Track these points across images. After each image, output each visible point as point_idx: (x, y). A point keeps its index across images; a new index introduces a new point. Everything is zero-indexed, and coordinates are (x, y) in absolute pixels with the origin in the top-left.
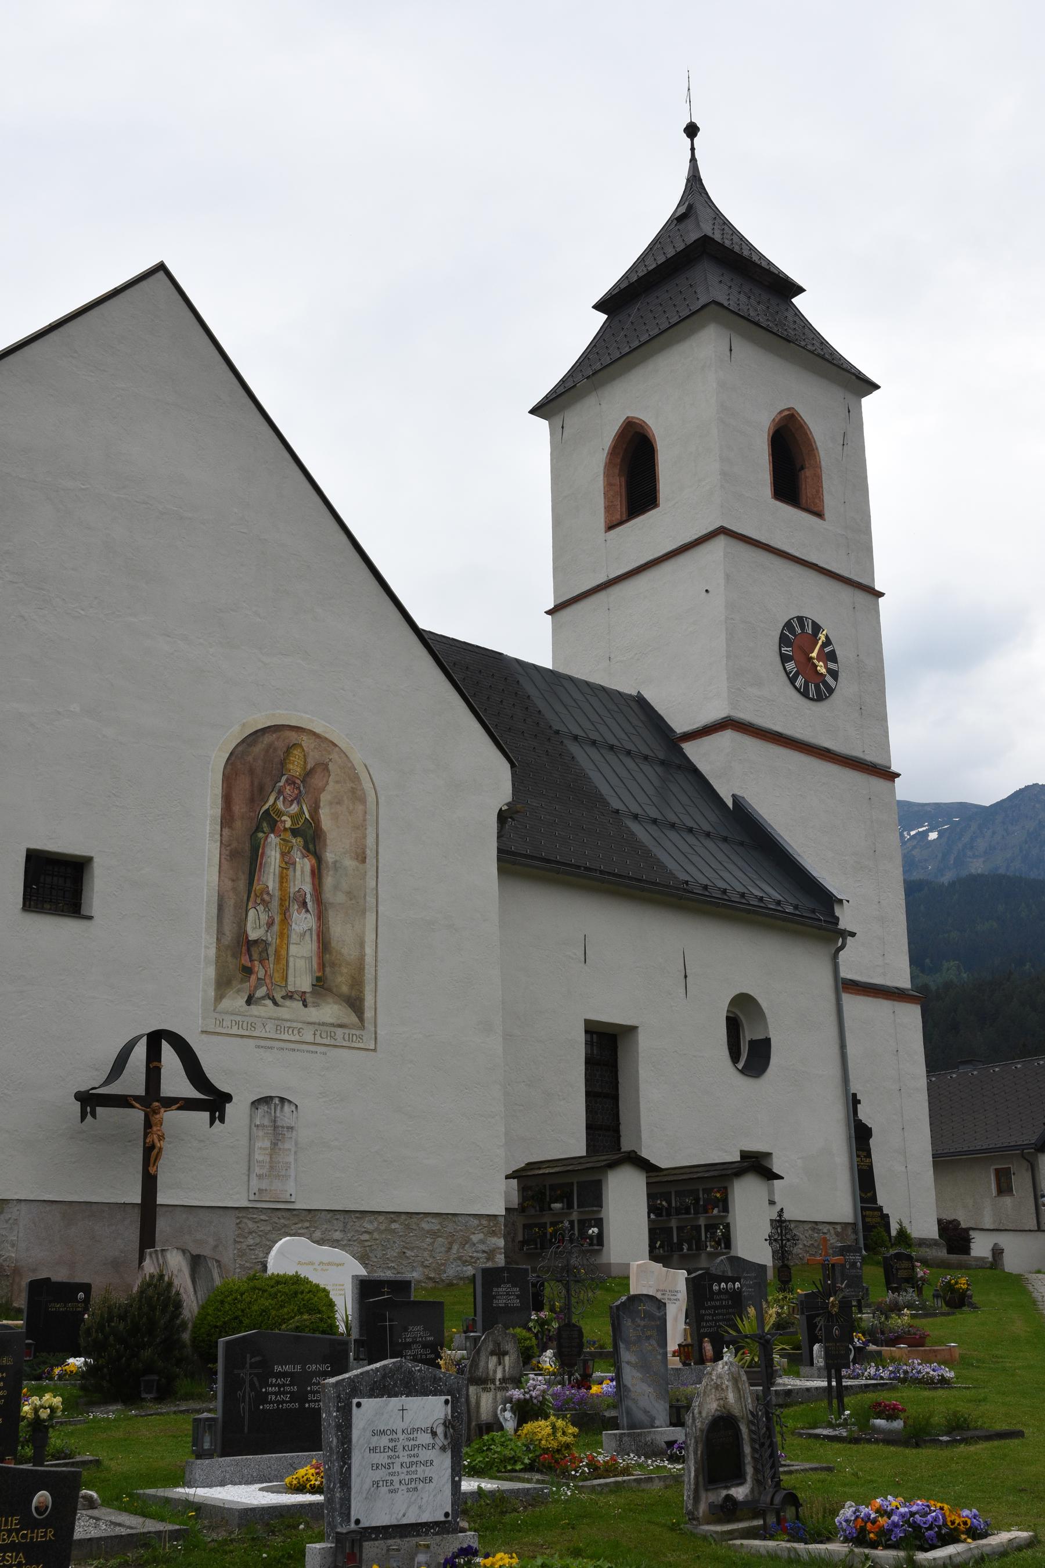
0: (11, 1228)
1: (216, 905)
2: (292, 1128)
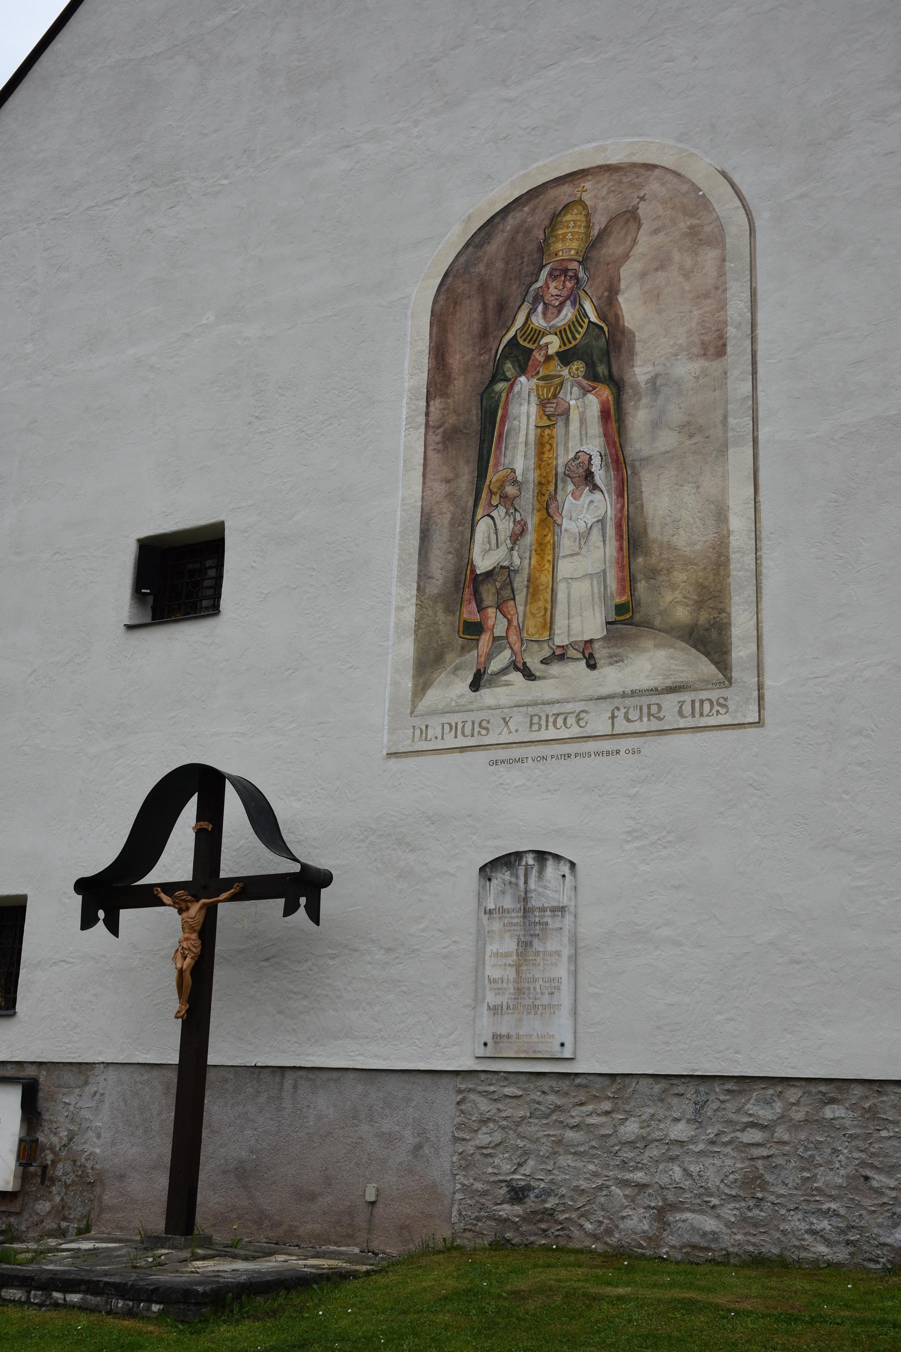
0: (97, 1108)
1: (417, 534)
2: (563, 909)
